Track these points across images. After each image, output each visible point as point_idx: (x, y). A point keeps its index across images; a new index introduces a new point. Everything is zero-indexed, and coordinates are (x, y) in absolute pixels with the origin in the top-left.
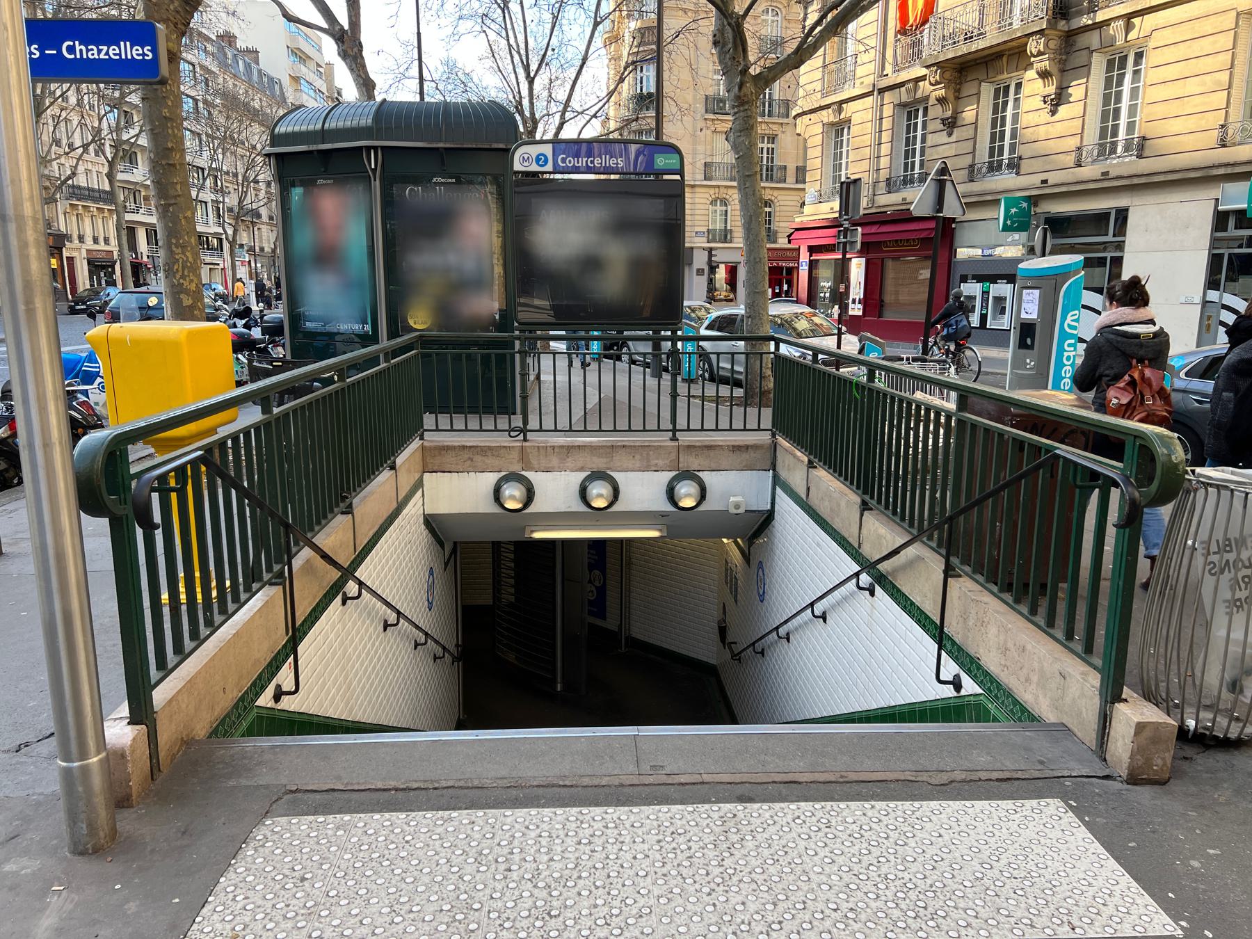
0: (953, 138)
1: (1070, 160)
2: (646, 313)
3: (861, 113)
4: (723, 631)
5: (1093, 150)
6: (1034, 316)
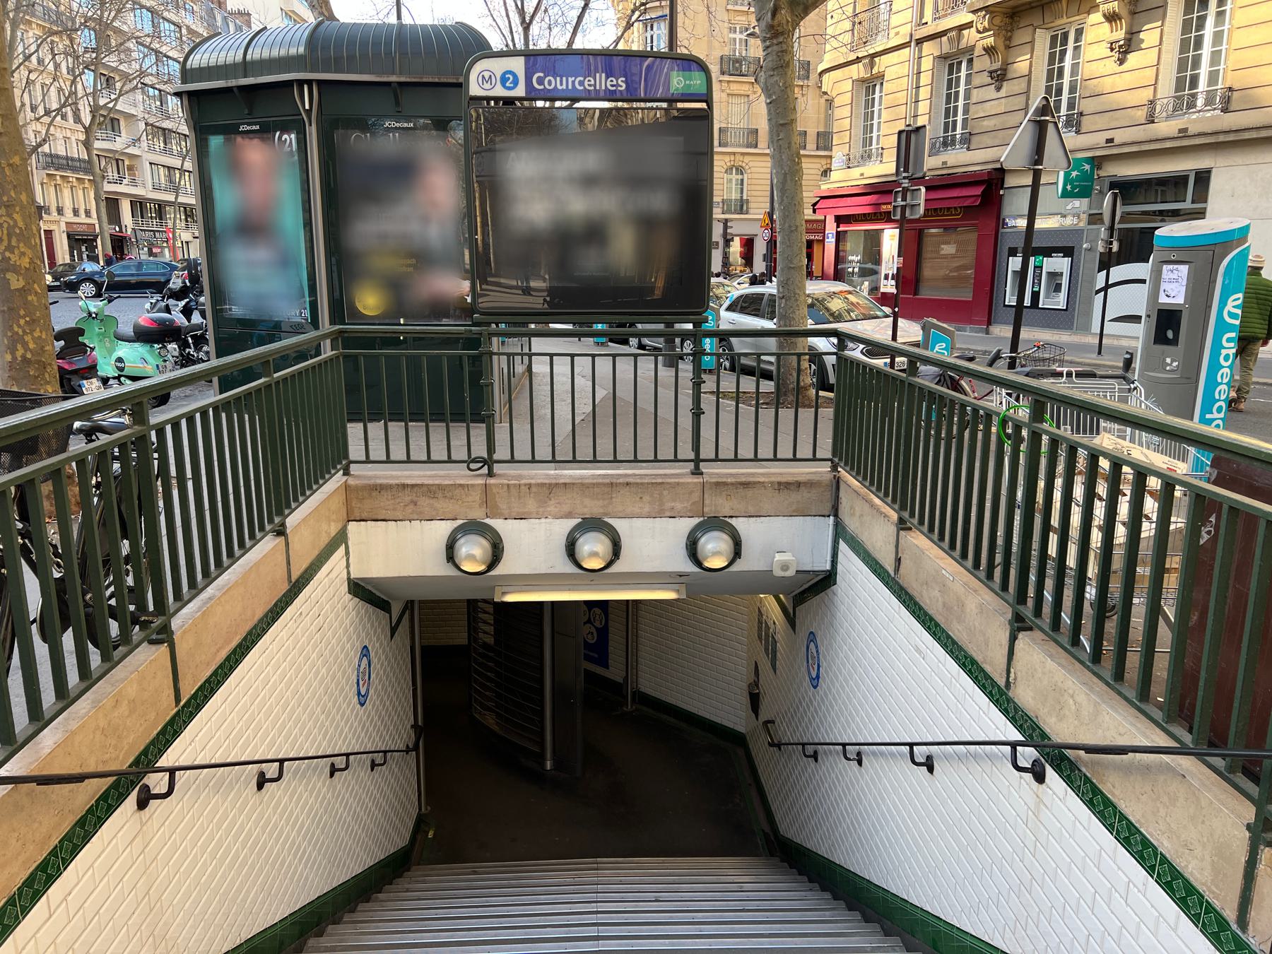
0: (1003, 93)
1: (1141, 114)
2: (658, 294)
3: (895, 67)
4: (755, 701)
5: (1168, 104)
6: (1180, 300)
